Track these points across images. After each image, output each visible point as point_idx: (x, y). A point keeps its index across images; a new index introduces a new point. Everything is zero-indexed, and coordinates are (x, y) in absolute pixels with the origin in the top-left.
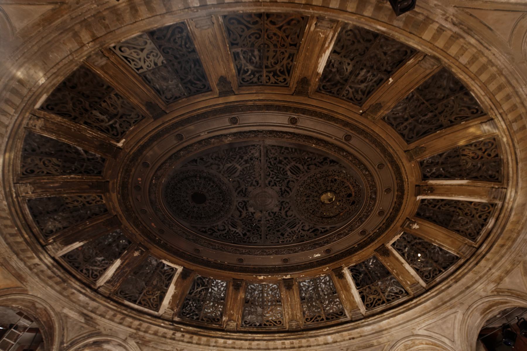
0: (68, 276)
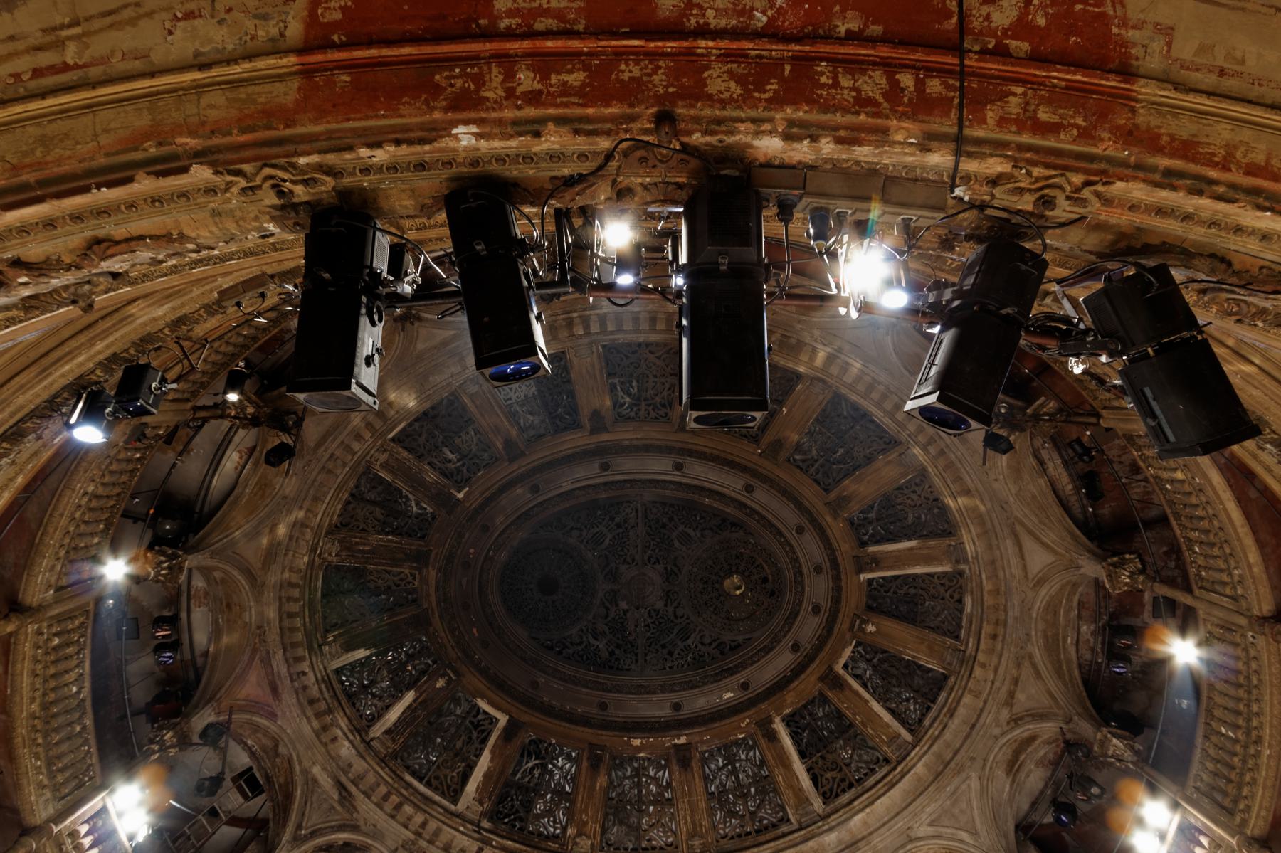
0: (336, 704)
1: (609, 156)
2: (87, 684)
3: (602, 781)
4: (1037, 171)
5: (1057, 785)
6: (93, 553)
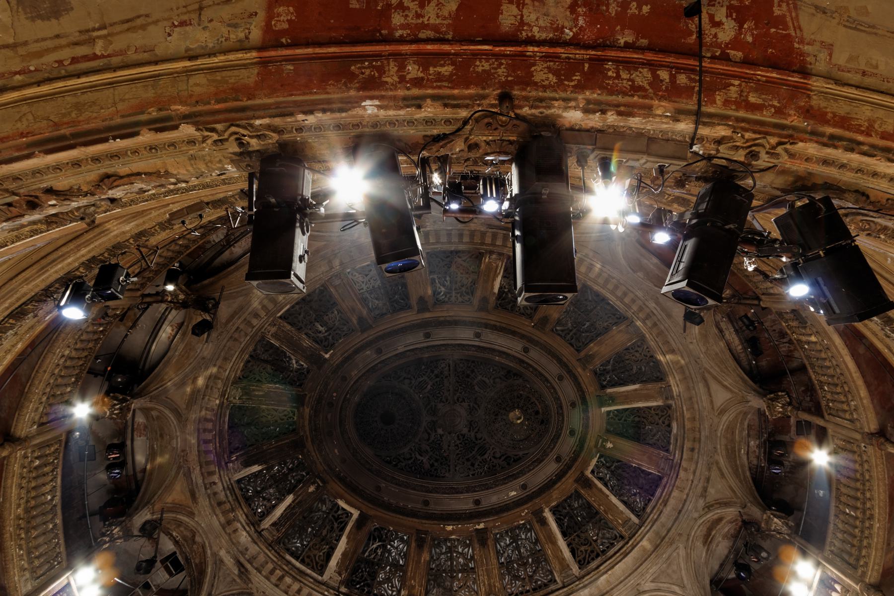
1: (466, 122)
2: (59, 494)
3: (425, 556)
4: (748, 135)
5: (737, 552)
6: (66, 398)
